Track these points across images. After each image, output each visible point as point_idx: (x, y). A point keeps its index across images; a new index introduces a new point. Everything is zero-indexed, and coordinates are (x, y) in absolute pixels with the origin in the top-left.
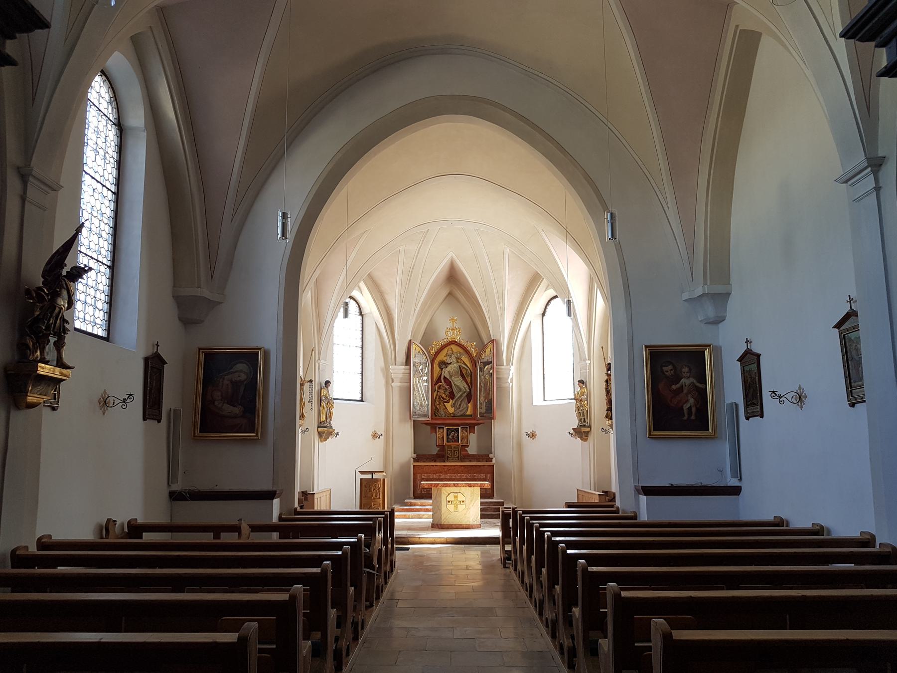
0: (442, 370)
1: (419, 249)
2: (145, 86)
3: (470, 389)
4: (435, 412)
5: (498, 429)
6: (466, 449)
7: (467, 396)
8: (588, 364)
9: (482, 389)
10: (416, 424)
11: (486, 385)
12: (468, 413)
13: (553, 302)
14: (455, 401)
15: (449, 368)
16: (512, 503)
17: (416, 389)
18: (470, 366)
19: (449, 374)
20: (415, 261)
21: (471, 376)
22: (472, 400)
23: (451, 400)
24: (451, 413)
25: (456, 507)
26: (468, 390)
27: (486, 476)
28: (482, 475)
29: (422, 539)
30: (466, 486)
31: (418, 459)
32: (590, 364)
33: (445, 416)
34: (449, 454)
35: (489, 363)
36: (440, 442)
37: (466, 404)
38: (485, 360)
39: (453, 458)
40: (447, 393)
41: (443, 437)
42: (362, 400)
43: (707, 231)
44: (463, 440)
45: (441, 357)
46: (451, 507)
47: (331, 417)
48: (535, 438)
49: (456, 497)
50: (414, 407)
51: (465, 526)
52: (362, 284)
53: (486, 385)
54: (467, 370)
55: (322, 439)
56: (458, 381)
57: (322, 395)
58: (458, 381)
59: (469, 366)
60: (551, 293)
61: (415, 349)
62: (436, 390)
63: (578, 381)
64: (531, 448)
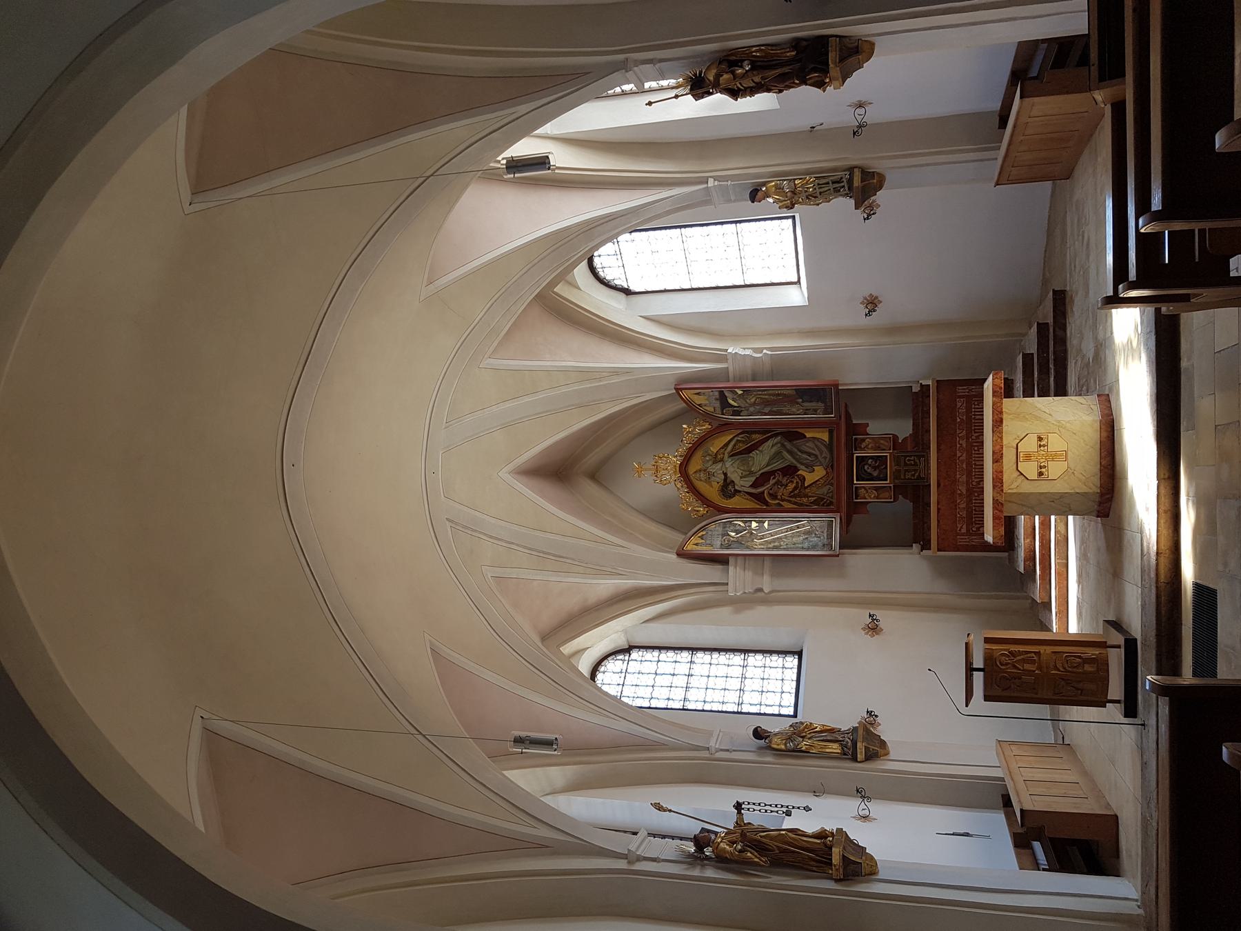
0: (740, 491)
1: (491, 537)
3: (776, 435)
4: (823, 505)
5: (857, 376)
8: (716, 183)
9: (775, 409)
10: (848, 543)
11: (766, 403)
12: (825, 436)
13: (608, 275)
14: (802, 464)
15: (734, 476)
16: (1024, 335)
17: (776, 544)
18: (732, 434)
19: (744, 477)
20: (517, 545)
23: (799, 473)
24: (825, 473)
25: (1054, 457)
27: (960, 397)
28: (959, 404)
29: (1162, 547)
30: (1001, 432)
32: (715, 178)
33: (832, 484)
34: (913, 475)
35: (722, 398)
36: (887, 494)
38: (718, 404)
39: (922, 466)
40: (784, 481)
41: (877, 489)
42: (800, 654)
43: (518, 52)
45: (712, 491)
46: (1055, 469)
47: (832, 731)
48: (876, 298)
49: (1028, 457)
50: (814, 547)
51: (1105, 434)
52: (567, 649)
53: (766, 403)
54: (737, 440)
55: (881, 751)
56: (761, 460)
57: (783, 747)
58: (761, 460)
59: (729, 438)
60: (581, 271)
61: (696, 544)
62: (779, 504)
63: (753, 202)
64: (893, 309)
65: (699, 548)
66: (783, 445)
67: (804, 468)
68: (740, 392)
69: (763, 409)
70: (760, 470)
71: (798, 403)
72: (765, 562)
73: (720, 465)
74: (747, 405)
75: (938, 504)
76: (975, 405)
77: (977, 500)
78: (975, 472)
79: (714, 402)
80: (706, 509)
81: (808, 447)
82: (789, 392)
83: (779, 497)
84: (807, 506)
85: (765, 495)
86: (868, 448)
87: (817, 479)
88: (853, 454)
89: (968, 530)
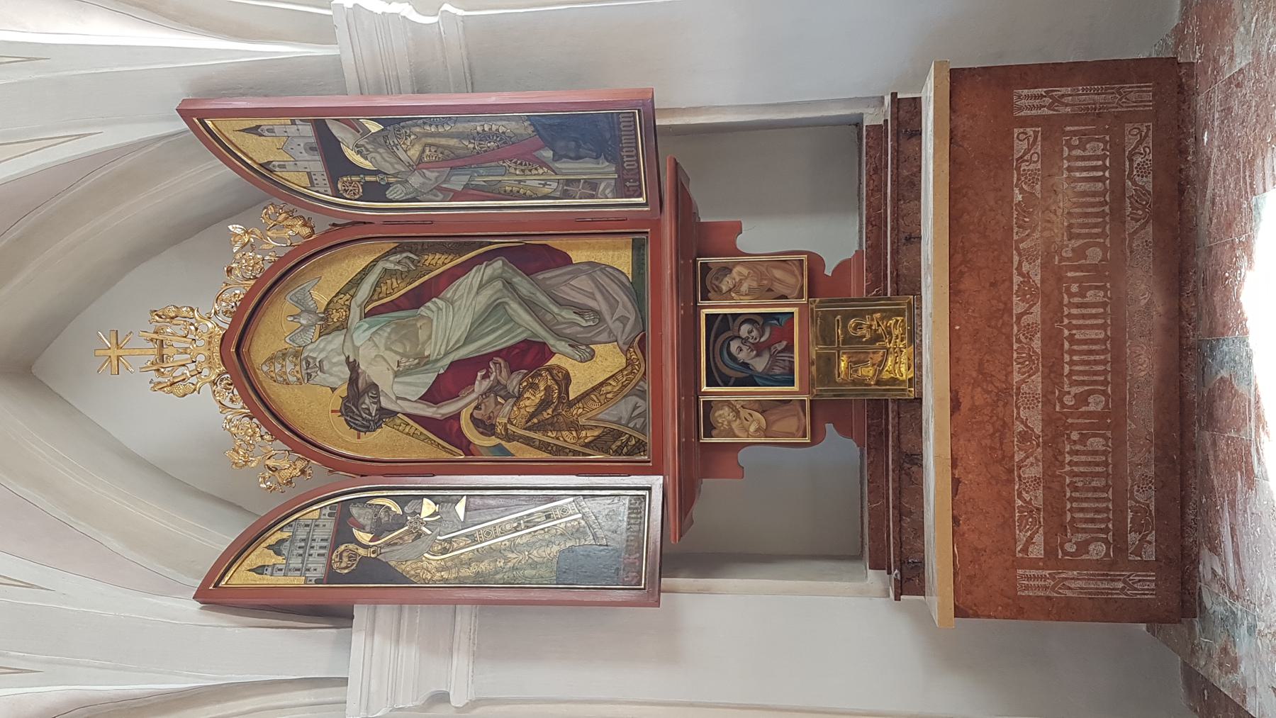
3: (490, 256)
4: (617, 452)
6: (828, 272)
9: (479, 181)
11: (454, 161)
12: (621, 259)
14: (559, 336)
15: (377, 371)
21: (421, 250)
22: (550, 242)
23: (553, 361)
24: (621, 361)
26: (498, 264)
27: (1024, 122)
28: (1020, 147)
31: (901, 564)
33: (642, 394)
36: (790, 424)
38: (317, 165)
41: (764, 408)
44: (781, 289)
61: (260, 570)
65: (267, 580)
66: (508, 284)
67: (569, 350)
68: (374, 127)
69: (445, 182)
70: (447, 354)
72: (458, 618)
73: (337, 340)
74: (400, 168)
75: (954, 465)
76: (1071, 148)
77: (1077, 453)
78: (1072, 352)
79: (306, 156)
80: (300, 464)
81: (574, 288)
82: (513, 125)
83: (499, 429)
84: (575, 453)
85: (463, 422)
86: (738, 293)
87: (601, 379)
88: (697, 310)
89: (1050, 551)
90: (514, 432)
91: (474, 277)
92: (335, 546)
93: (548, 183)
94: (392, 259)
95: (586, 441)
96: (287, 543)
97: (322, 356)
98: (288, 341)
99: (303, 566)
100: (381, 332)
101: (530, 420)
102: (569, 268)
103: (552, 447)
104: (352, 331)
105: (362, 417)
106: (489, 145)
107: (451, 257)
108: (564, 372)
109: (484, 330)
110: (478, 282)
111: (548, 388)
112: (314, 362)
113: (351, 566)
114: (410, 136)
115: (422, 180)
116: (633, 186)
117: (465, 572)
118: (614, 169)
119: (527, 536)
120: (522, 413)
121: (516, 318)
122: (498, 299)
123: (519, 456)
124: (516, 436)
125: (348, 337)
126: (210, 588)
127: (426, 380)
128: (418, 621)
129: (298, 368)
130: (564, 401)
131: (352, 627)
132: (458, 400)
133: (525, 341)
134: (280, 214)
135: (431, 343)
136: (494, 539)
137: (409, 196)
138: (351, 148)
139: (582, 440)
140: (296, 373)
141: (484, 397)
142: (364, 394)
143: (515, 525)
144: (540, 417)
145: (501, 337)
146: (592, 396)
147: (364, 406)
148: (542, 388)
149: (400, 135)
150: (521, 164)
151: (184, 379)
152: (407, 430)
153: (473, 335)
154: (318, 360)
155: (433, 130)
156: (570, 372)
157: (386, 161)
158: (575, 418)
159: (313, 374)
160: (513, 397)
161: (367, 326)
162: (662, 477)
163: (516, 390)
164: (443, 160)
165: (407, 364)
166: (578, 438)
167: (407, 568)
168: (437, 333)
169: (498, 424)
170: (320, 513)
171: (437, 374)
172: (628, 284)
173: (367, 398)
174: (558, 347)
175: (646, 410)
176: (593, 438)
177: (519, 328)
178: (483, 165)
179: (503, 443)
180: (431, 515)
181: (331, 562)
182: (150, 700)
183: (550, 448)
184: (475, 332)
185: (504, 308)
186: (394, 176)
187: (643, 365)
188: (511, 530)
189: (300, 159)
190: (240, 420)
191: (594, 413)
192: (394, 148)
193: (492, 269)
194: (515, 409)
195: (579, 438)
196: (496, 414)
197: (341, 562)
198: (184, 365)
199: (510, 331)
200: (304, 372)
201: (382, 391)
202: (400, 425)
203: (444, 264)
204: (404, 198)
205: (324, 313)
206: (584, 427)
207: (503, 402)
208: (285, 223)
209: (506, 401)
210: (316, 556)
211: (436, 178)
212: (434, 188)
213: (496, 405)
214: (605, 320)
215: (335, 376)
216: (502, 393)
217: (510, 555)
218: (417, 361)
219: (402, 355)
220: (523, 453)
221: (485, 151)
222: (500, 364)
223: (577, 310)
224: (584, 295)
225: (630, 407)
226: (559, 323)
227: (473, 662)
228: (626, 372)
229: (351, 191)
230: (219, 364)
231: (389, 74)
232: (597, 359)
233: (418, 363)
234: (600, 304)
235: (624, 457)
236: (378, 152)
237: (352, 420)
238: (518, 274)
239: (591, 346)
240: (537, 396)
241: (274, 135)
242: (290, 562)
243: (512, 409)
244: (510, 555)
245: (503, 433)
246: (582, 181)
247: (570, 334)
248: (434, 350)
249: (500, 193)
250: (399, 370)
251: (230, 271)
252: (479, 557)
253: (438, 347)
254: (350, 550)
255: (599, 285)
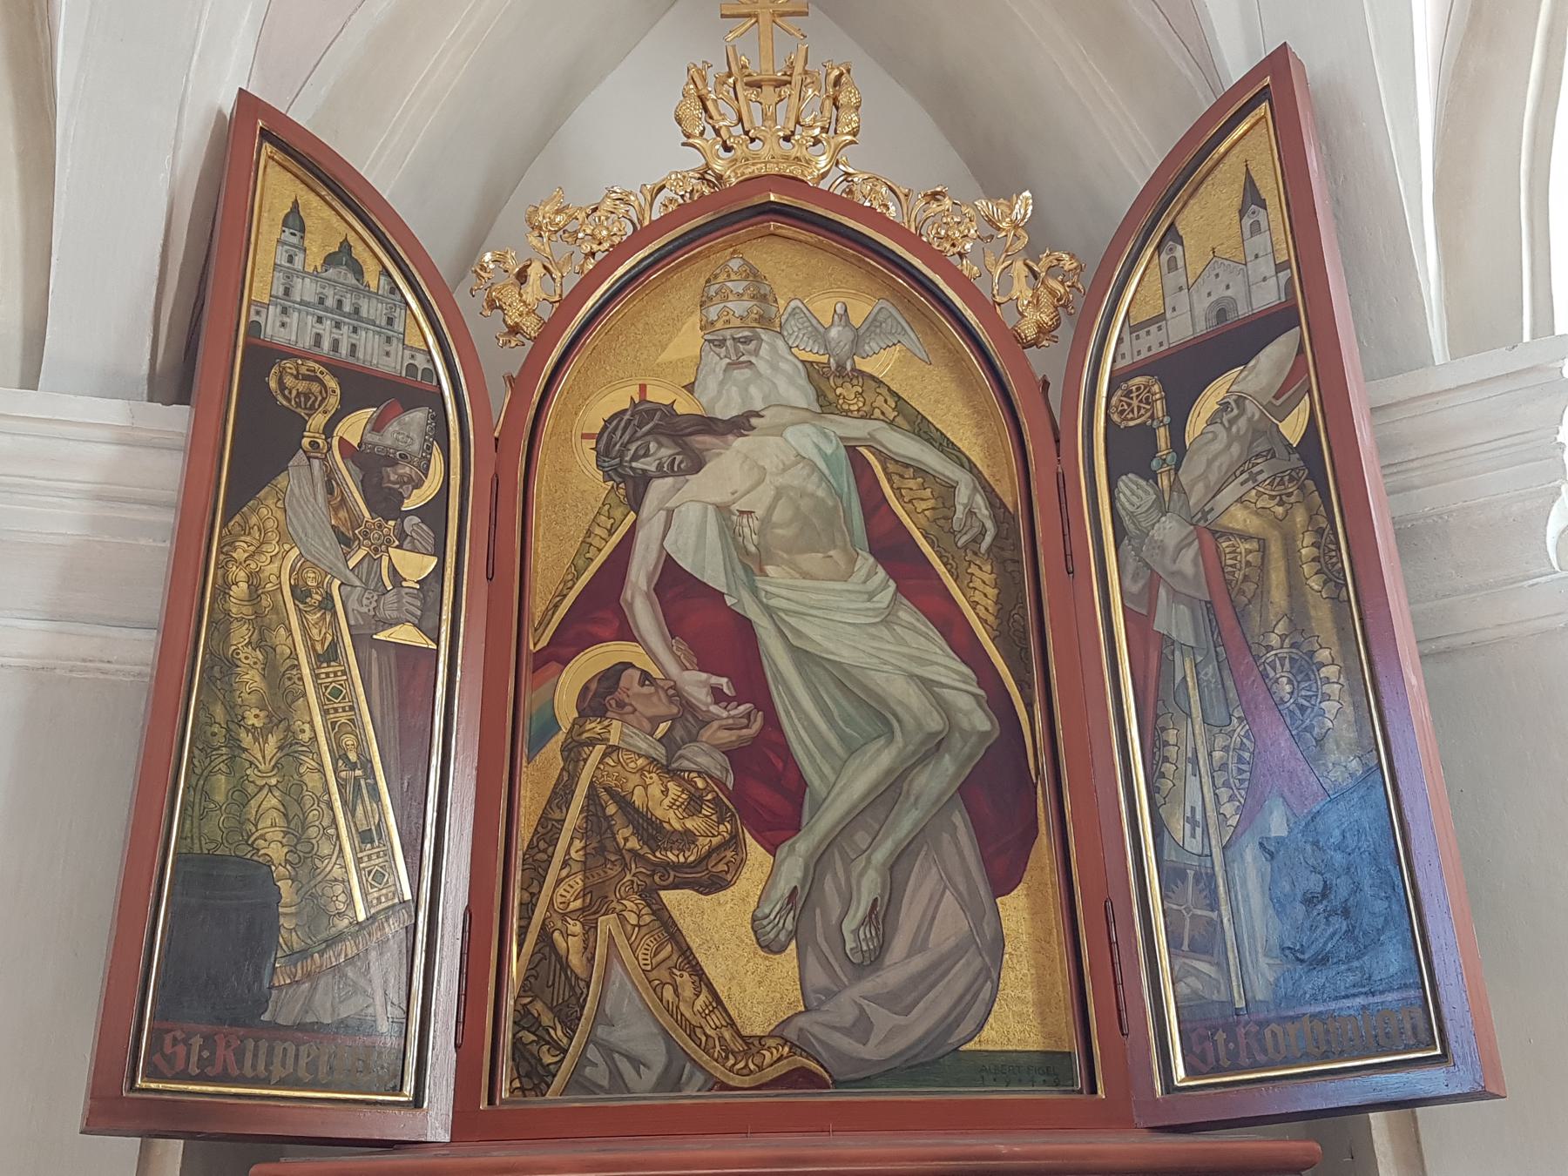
0: (636, 503)
2: (199, 277)
3: (998, 702)
4: (524, 1018)
7: (967, 791)
9: (1184, 668)
14: (817, 865)
18: (990, 452)
22: (1044, 850)
23: (755, 850)
24: (756, 1022)
26: (981, 722)
33: (671, 1080)
37: (967, 904)
38: (1183, 328)
54: (952, 487)
61: (295, 220)
62: (552, 726)
66: (935, 746)
67: (783, 888)
68: (1293, 428)
69: (1174, 594)
70: (769, 611)
71: (1251, 811)
73: (798, 394)
79: (1203, 304)
81: (935, 902)
83: (594, 727)
87: (710, 971)
90: (585, 760)
91: (945, 667)
92: (335, 369)
93: (1199, 831)
94: (979, 500)
95: (556, 934)
96: (351, 279)
97: (762, 366)
98: (793, 304)
99: (294, 302)
100: (815, 478)
101: (612, 798)
102: (983, 890)
103: (545, 851)
104: (816, 423)
105: (628, 442)
106: (1285, 680)
107: (991, 619)
108: (729, 877)
109: (828, 693)
110: (936, 678)
111: (688, 837)
112: (750, 353)
113: (285, 397)
114: (1281, 503)
115: (1171, 543)
116: (1216, 1050)
117: (241, 635)
118: (1260, 997)
119: (319, 785)
120: (633, 776)
121: (858, 761)
122: (899, 721)
123: (526, 773)
124: (576, 767)
125: (808, 414)
126: (260, 121)
127: (713, 572)
128: (143, 542)
129: (738, 323)
130: (656, 878)
131: (150, 400)
132: (663, 635)
133: (802, 784)
134: (1062, 283)
135: (793, 578)
136: (321, 705)
137: (1127, 521)
138: (1234, 388)
139: (559, 924)
140: (725, 318)
141: (671, 692)
142: (680, 446)
143: (353, 757)
144: (618, 821)
145: (811, 727)
146: (669, 948)
147: (653, 446)
148: (689, 824)
149: (1282, 482)
150: (1240, 760)
151: (711, 118)
152: (597, 531)
153: (816, 669)
154: (753, 360)
155: (1304, 551)
156: (729, 892)
157: (1210, 463)
158: (614, 905)
159: (723, 351)
160: (670, 757)
161: (829, 452)
162: (447, 1139)
163: (686, 764)
164: (1227, 582)
165: (747, 530)
166: (565, 914)
167: (266, 510)
168: (817, 590)
169: (606, 723)
170: (418, 350)
171: (725, 591)
172: (953, 1040)
173: (670, 452)
174: (788, 860)
175: (629, 1092)
176: (563, 952)
177: (833, 768)
178: (1226, 673)
179: (561, 737)
180: (395, 569)
181: (301, 358)
182: (43, 31)
183: (542, 845)
184: (821, 672)
185: (879, 736)
186: (1175, 485)
187: (747, 1081)
188: (339, 745)
189: (1195, 297)
190: (626, 216)
191: (626, 953)
192: (1245, 476)
193: (968, 708)
194: (641, 762)
195: (564, 916)
196: (630, 718)
197: (296, 377)
198: (740, 120)
199: (826, 748)
200: (728, 334)
201: (687, 481)
202: (609, 518)
203: (974, 605)
204: (1122, 513)
205: (854, 369)
206: (590, 928)
207: (659, 733)
208: (1042, 290)
209: (659, 740)
210: (315, 330)
211: (1178, 574)
212: (1152, 570)
213: (650, 719)
214: (859, 978)
215: (720, 392)
216: (679, 733)
217: (272, 741)
218: (753, 549)
219: (766, 521)
220: (532, 782)
221: (1264, 676)
222: (747, 727)
223: (880, 909)
224: (919, 927)
225: (639, 1048)
226: (848, 863)
227: (27, 668)
228: (727, 1035)
229: (1129, 405)
230: (743, 174)
231: (1413, 470)
232: (761, 960)
233: (748, 553)
234: (898, 969)
235: (509, 1035)
236: (1229, 446)
237: (623, 424)
238: (962, 766)
239: (793, 944)
240: (671, 814)
241: (1245, 237)
242: (307, 280)
243: (640, 756)
244: (272, 741)
245: (585, 735)
246: (1214, 915)
247: (823, 889)
248: (778, 586)
249: (1157, 717)
250: (732, 513)
251: (935, 196)
252: (280, 679)
253: (784, 592)
254: (323, 399)
255: (943, 967)
